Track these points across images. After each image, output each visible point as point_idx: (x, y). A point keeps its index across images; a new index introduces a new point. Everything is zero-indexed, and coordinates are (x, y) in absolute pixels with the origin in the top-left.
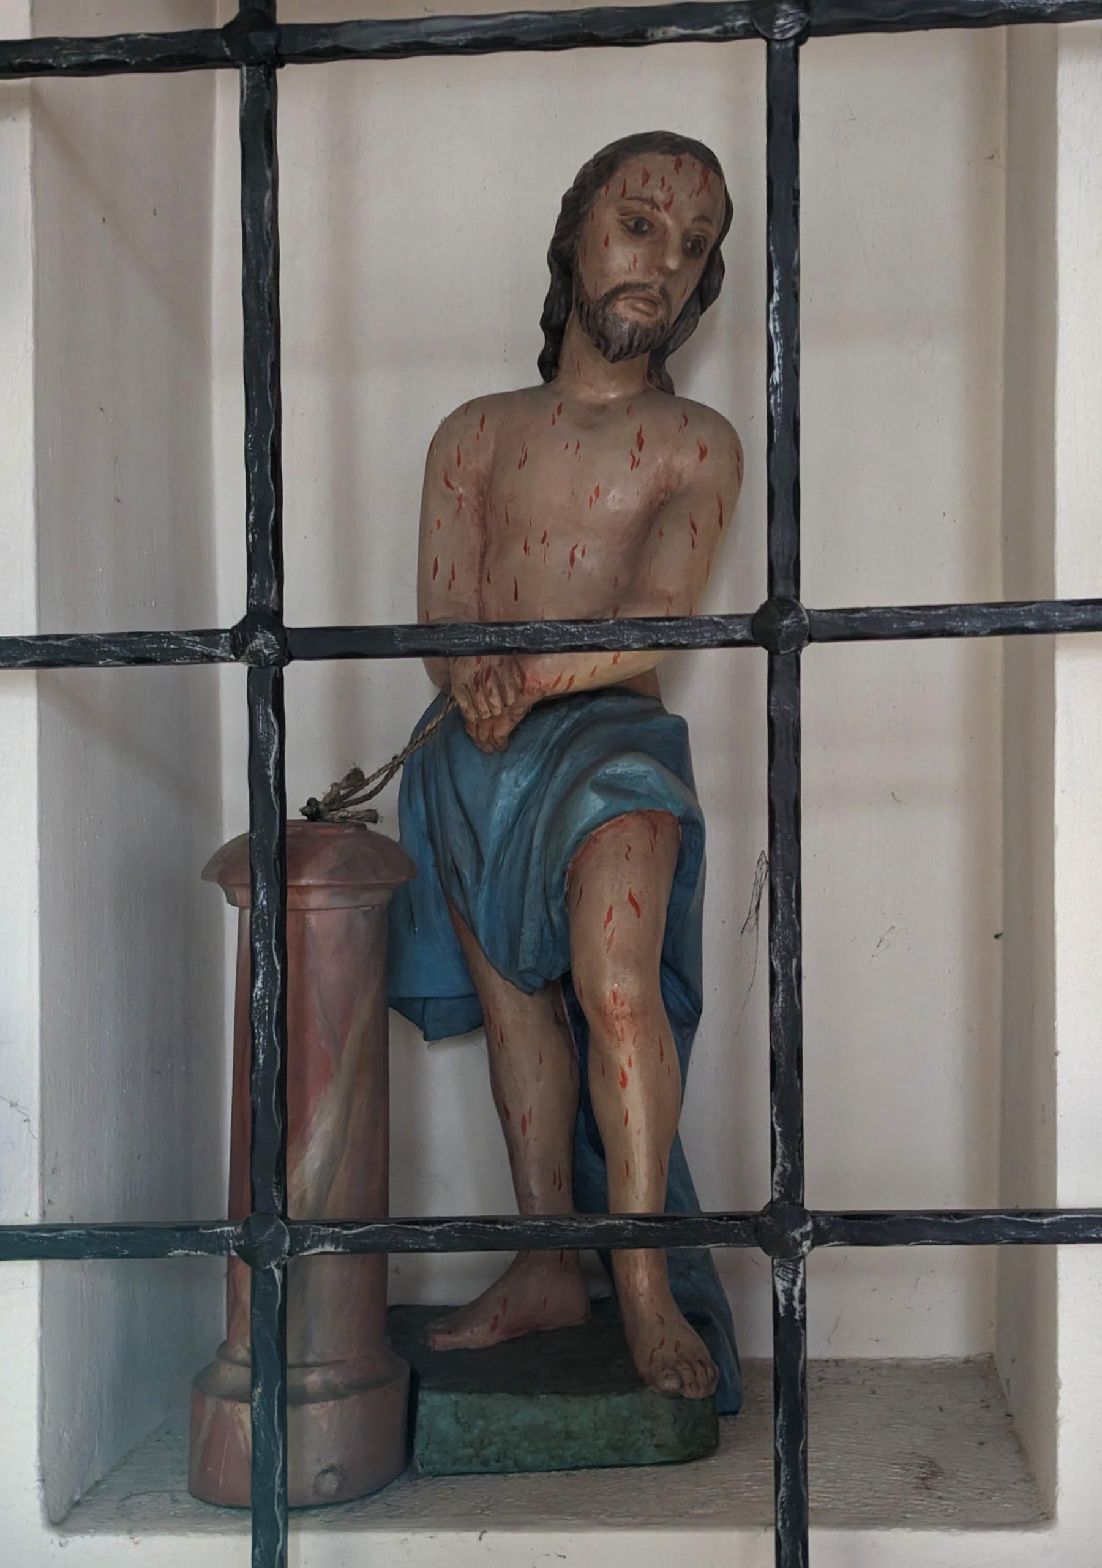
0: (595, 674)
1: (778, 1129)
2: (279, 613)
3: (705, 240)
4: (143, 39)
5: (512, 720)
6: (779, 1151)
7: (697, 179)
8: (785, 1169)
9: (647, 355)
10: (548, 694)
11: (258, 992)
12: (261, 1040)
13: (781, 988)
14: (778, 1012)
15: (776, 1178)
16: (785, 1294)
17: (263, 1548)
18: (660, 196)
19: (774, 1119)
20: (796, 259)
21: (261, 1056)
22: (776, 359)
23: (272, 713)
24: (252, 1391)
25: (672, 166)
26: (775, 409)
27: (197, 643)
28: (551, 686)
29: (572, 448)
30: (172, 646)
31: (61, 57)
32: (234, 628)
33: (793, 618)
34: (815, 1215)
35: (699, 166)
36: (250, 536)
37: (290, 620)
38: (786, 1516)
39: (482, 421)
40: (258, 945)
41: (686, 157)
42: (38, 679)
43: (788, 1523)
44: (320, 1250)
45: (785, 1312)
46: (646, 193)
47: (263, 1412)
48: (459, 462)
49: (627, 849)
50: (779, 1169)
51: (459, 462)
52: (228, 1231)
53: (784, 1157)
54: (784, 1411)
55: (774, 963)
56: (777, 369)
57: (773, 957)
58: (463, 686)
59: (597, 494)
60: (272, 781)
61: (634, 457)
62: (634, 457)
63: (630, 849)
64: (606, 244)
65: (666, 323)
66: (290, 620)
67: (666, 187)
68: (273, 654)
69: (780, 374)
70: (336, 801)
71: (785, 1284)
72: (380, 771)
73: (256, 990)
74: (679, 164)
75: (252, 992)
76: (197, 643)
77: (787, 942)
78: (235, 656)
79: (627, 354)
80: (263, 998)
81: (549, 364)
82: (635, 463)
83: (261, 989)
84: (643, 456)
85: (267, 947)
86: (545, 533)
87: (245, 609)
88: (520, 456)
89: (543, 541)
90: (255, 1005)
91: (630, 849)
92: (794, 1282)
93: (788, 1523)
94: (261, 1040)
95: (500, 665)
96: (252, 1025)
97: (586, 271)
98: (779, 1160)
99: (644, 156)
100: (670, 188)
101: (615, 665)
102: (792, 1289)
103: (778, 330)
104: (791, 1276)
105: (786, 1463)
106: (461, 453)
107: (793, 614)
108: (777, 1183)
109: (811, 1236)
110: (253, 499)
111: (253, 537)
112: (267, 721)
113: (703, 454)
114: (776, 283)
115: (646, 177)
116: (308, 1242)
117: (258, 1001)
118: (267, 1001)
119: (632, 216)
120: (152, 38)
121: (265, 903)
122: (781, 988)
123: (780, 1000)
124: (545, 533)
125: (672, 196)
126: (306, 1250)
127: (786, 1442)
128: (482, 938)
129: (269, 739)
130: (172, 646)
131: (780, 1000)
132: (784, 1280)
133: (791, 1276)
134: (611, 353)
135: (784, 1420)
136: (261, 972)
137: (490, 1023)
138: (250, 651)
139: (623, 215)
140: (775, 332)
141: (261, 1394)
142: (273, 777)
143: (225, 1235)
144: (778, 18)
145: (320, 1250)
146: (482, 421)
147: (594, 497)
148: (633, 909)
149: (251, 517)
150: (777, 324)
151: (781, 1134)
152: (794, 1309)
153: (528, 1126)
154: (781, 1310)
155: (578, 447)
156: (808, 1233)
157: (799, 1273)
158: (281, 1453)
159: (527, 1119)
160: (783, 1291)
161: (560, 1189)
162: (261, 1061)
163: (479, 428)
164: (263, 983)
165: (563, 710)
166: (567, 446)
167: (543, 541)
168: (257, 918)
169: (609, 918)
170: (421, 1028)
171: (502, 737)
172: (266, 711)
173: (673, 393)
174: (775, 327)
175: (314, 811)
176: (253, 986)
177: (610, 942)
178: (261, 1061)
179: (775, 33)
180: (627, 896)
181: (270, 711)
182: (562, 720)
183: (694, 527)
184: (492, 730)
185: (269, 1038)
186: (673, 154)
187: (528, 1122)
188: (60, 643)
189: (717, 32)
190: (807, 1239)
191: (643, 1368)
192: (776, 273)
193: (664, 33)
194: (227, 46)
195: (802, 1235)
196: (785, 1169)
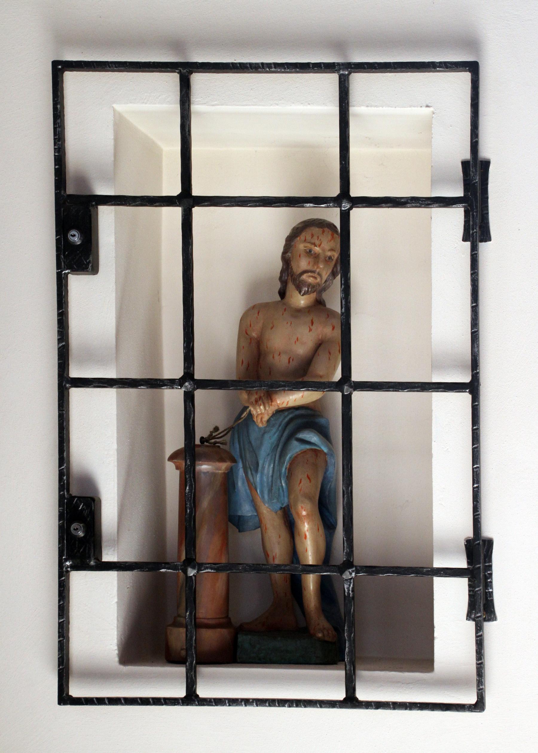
0: (296, 401)
1: (345, 539)
2: (193, 375)
3: (333, 256)
4: (152, 198)
5: (268, 415)
6: (345, 545)
7: (330, 237)
8: (347, 551)
9: (315, 293)
10: (280, 407)
11: (187, 491)
12: (188, 505)
13: (346, 496)
14: (345, 503)
15: (344, 554)
16: (347, 589)
17: (189, 662)
18: (317, 242)
19: (344, 536)
20: (349, 275)
21: (188, 511)
22: (343, 305)
23: (191, 405)
24: (186, 614)
25: (321, 232)
26: (343, 320)
27: (169, 383)
28: (281, 404)
29: (289, 323)
30: (161, 383)
31: (127, 202)
32: (180, 378)
33: (348, 383)
34: (356, 566)
35: (330, 233)
36: (185, 351)
37: (196, 377)
38: (348, 657)
39: (259, 313)
40: (187, 476)
41: (326, 229)
42: (117, 392)
43: (348, 659)
44: (206, 571)
45: (347, 594)
46: (313, 241)
47: (189, 620)
48: (250, 326)
49: (307, 461)
50: (345, 551)
51: (250, 326)
52: (178, 564)
53: (347, 547)
54: (347, 625)
55: (344, 489)
56: (343, 308)
57: (343, 486)
58: (251, 402)
59: (295, 342)
60: (191, 426)
61: (310, 328)
62: (310, 328)
63: (308, 460)
64: (300, 256)
65: (320, 283)
66: (196, 377)
67: (319, 239)
68: (192, 387)
69: (344, 310)
70: (211, 437)
71: (347, 586)
72: (225, 430)
73: (186, 490)
74: (323, 232)
75: (185, 490)
76: (169, 383)
77: (347, 482)
78: (180, 387)
79: (307, 293)
80: (189, 492)
81: (282, 294)
82: (310, 330)
83: (188, 490)
84: (313, 328)
85: (190, 477)
86: (280, 353)
87: (183, 373)
88: (271, 325)
89: (279, 355)
90: (186, 494)
91: (308, 460)
92: (350, 586)
93: (348, 659)
94: (188, 505)
95: (264, 396)
96: (185, 501)
97: (294, 264)
98: (345, 548)
99: (312, 228)
100: (320, 240)
101: (302, 398)
102: (349, 588)
103: (343, 296)
104: (349, 584)
105: (348, 640)
106: (252, 323)
107: (348, 382)
108: (345, 555)
109: (355, 571)
110: (185, 339)
111: (185, 351)
112: (190, 407)
113: (333, 328)
114: (343, 282)
115: (312, 236)
116: (203, 568)
117: (187, 493)
118: (190, 494)
119: (308, 248)
120: (155, 197)
121: (189, 463)
122: (346, 496)
123: (345, 499)
124: (280, 353)
125: (321, 243)
126: (202, 571)
127: (347, 634)
128: (259, 493)
129: (190, 414)
130: (161, 383)
131: (345, 499)
132: (347, 585)
133: (349, 584)
134: (302, 294)
135: (347, 627)
136: (188, 485)
137: (262, 523)
138: (185, 386)
139: (305, 247)
140: (343, 297)
141: (188, 615)
142: (191, 425)
143: (178, 565)
144: (343, 204)
145: (206, 571)
146: (259, 313)
147: (296, 341)
148: (308, 480)
149: (185, 345)
150: (343, 294)
151: (346, 540)
152: (350, 594)
153: (275, 559)
154: (346, 594)
155: (291, 323)
156: (354, 570)
157: (351, 583)
158: (195, 633)
159: (275, 557)
160: (347, 588)
161: (286, 582)
162: (188, 512)
163: (257, 314)
164: (189, 488)
165: (286, 413)
166: (287, 323)
167: (279, 355)
168: (187, 468)
169: (301, 482)
170: (237, 528)
171: (265, 421)
172: (189, 404)
173: (325, 306)
174: (343, 296)
175: (202, 440)
176: (186, 489)
177: (300, 490)
178: (188, 512)
179: (342, 208)
180: (306, 476)
181: (190, 404)
182: (285, 417)
183: (330, 353)
184: (261, 419)
185: (190, 504)
186: (322, 228)
187: (275, 558)
188: (126, 381)
189: (325, 206)
190: (354, 572)
191: (312, 632)
192: (343, 279)
193: (309, 205)
194: (178, 202)
195: (352, 571)
196: (347, 551)
